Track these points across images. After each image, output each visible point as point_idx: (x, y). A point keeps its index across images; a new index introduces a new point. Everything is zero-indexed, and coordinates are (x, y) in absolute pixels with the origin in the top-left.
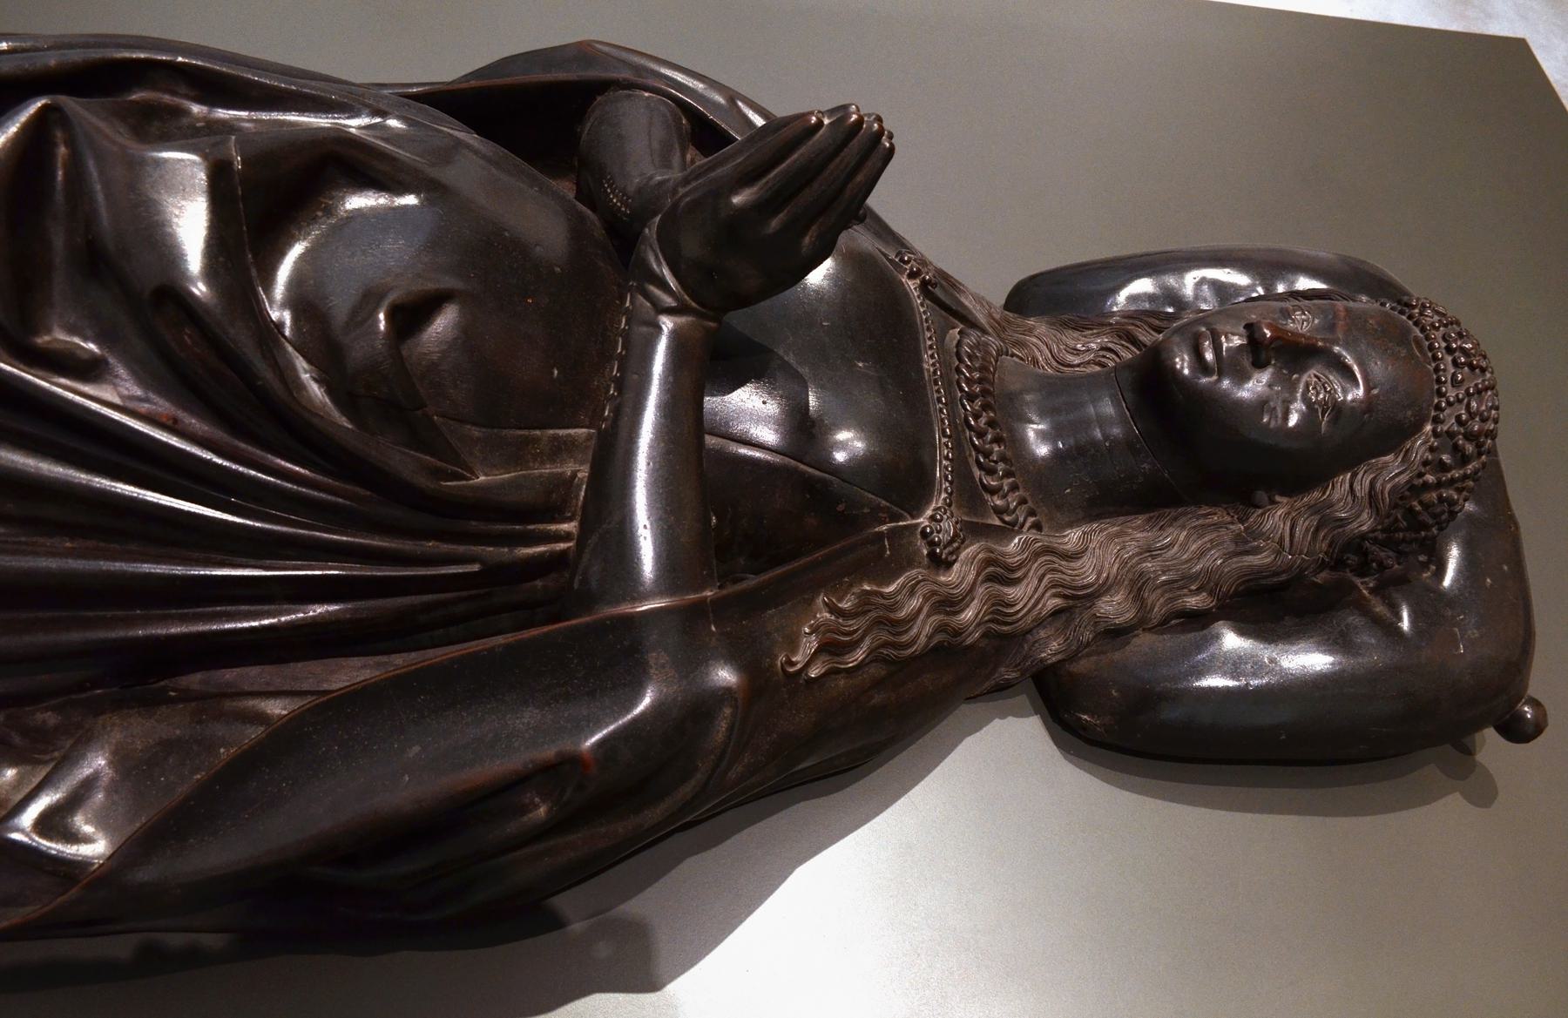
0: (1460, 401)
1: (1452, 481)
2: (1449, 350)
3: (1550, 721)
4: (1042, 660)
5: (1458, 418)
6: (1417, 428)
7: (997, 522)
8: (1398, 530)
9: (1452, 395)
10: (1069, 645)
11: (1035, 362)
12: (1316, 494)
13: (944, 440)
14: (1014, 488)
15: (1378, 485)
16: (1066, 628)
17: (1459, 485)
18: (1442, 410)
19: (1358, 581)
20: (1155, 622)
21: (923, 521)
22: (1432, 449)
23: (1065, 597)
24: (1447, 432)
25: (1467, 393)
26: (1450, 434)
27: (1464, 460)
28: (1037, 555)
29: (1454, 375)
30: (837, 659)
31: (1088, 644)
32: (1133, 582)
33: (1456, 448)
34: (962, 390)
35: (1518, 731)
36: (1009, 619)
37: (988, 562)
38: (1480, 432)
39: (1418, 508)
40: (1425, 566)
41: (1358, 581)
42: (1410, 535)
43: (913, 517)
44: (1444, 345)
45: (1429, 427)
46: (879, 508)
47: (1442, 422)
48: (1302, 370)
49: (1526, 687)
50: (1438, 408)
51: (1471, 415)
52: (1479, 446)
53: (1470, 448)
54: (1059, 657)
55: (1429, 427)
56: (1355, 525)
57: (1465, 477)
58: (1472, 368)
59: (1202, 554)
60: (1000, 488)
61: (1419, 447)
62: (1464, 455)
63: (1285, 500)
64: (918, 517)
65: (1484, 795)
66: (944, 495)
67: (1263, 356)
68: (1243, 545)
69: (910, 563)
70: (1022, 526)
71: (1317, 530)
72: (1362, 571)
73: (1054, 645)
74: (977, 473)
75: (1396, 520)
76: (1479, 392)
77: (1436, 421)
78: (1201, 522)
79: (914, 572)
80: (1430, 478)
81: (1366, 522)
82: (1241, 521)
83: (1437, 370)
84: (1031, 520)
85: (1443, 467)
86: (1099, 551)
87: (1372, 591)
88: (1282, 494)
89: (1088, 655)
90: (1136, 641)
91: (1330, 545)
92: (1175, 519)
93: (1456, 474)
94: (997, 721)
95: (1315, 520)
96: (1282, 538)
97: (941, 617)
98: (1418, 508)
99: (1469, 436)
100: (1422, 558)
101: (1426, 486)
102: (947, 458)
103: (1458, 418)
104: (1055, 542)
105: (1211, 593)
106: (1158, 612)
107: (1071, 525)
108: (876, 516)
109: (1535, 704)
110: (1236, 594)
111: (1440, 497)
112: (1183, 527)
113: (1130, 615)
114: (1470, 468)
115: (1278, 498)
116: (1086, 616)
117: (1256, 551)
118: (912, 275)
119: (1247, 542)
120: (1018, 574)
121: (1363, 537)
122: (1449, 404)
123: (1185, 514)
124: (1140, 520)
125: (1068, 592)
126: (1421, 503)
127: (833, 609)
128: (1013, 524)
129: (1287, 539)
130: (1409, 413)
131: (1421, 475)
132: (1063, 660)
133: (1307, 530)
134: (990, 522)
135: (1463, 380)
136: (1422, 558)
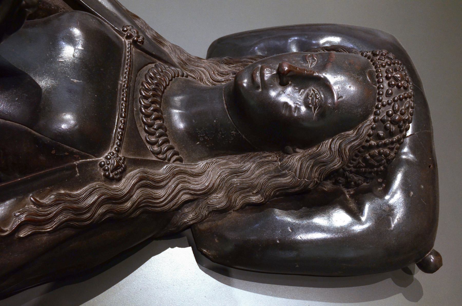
0: (389, 104)
1: (385, 145)
2: (387, 78)
3: (444, 262)
4: (185, 223)
5: (387, 113)
6: (365, 117)
7: (154, 158)
8: (361, 167)
9: (385, 100)
10: (198, 217)
11: (201, 80)
12: (315, 149)
13: (121, 119)
14: (166, 141)
15: (343, 146)
16: (196, 208)
17: (390, 146)
18: (379, 109)
19: (345, 191)
20: (238, 207)
21: (102, 159)
22: (372, 128)
23: (191, 194)
24: (381, 120)
25: (394, 100)
26: (383, 121)
27: (391, 134)
28: (174, 175)
29: (388, 91)
30: (38, 227)
31: (206, 217)
32: (227, 188)
33: (386, 129)
34: (141, 94)
35: (428, 268)
36: (158, 205)
37: (141, 179)
38: (399, 120)
39: (368, 157)
40: (380, 184)
41: (345, 191)
42: (368, 170)
43: (96, 157)
44: (385, 75)
45: (372, 117)
46: (75, 153)
47: (378, 115)
48: (286, 88)
49: (432, 245)
50: (377, 107)
51: (395, 112)
52: (400, 127)
53: (393, 128)
54: (194, 221)
55: (372, 117)
56: (331, 165)
57: (392, 143)
58: (399, 87)
59: (258, 177)
60: (157, 142)
61: (366, 127)
62: (390, 132)
63: (301, 151)
64: (100, 156)
65: (416, 295)
66: (115, 146)
67: (285, 79)
68: (279, 172)
69: (92, 179)
70: (169, 160)
71: (313, 167)
72: (348, 185)
73: (191, 216)
74: (143, 135)
75: (359, 163)
76: (401, 99)
77: (376, 114)
78: (263, 160)
79: (95, 183)
80: (373, 143)
81: (337, 164)
82: (280, 160)
83: (379, 88)
84: (175, 157)
85: (378, 137)
86: (210, 172)
87: (351, 196)
88: (300, 148)
89: (208, 221)
90: (229, 216)
91: (319, 175)
92: (251, 158)
93: (387, 141)
94: (170, 248)
95: (312, 162)
96: (296, 170)
97: (110, 205)
98: (368, 157)
99: (393, 122)
100: (380, 180)
101: (371, 147)
102: (120, 128)
103: (387, 113)
104: (188, 168)
105: (262, 196)
106: (239, 202)
107: (201, 159)
108: (73, 156)
109: (437, 254)
110: (275, 196)
111: (379, 152)
112: (254, 162)
113: (223, 204)
114: (395, 138)
115: (298, 150)
116: (204, 202)
117: (284, 176)
118: (128, 37)
119: (280, 171)
120: (162, 184)
121: (337, 171)
122: (383, 105)
123: (256, 155)
124: (237, 158)
125: (192, 192)
126: (369, 155)
127: (37, 204)
128: (164, 159)
129: (298, 172)
130: (360, 110)
131: (367, 141)
132: (196, 223)
133: (308, 167)
134: (149, 158)
135: (391, 94)
136: (380, 180)
